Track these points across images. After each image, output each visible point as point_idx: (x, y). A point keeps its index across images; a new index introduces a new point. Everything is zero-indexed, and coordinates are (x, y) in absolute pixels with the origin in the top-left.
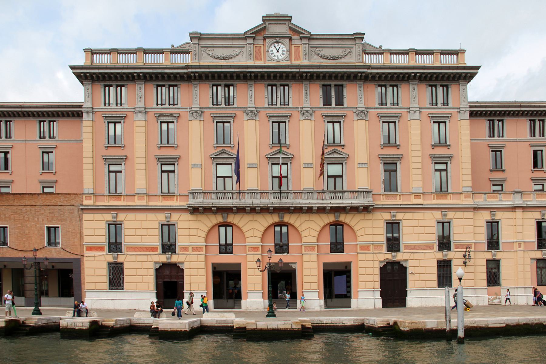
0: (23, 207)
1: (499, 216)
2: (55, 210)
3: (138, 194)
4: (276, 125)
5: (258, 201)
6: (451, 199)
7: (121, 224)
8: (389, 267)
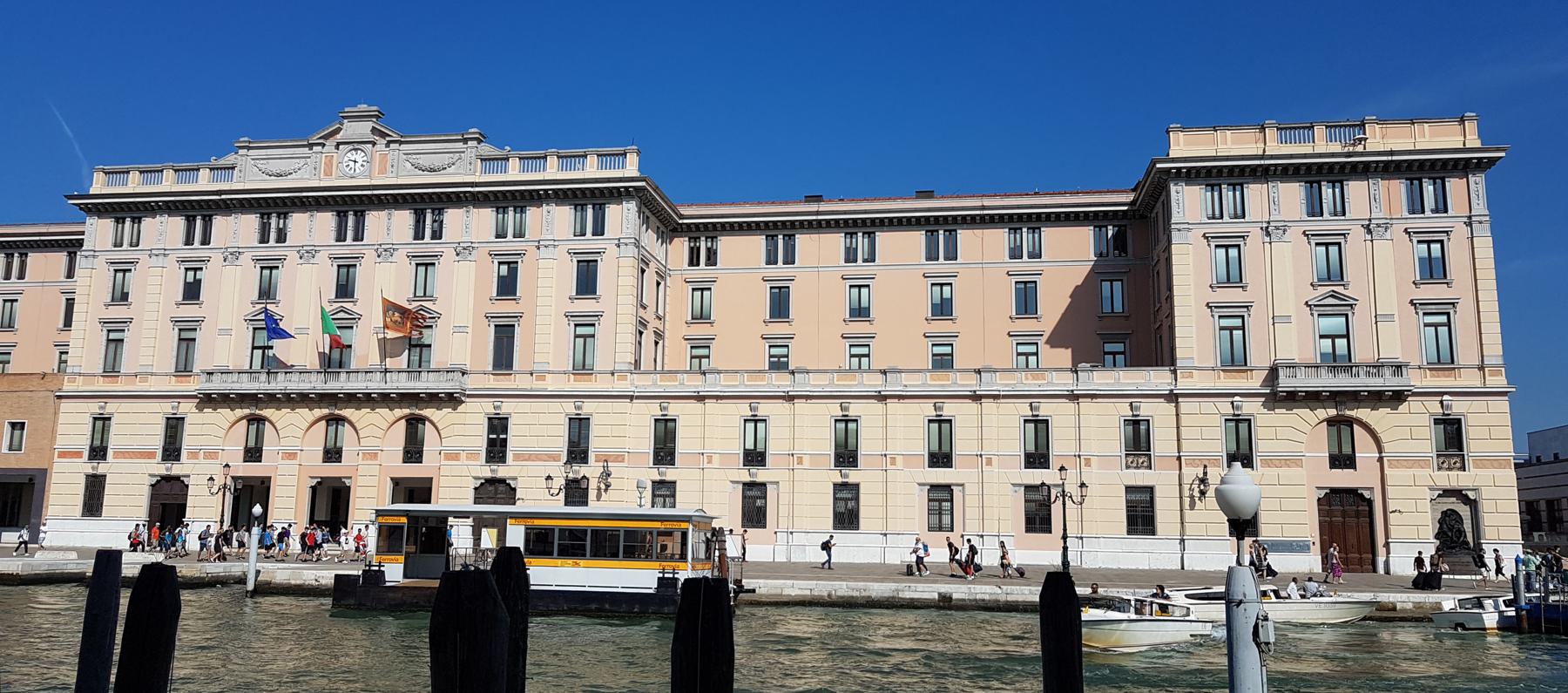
3: (141, 373)
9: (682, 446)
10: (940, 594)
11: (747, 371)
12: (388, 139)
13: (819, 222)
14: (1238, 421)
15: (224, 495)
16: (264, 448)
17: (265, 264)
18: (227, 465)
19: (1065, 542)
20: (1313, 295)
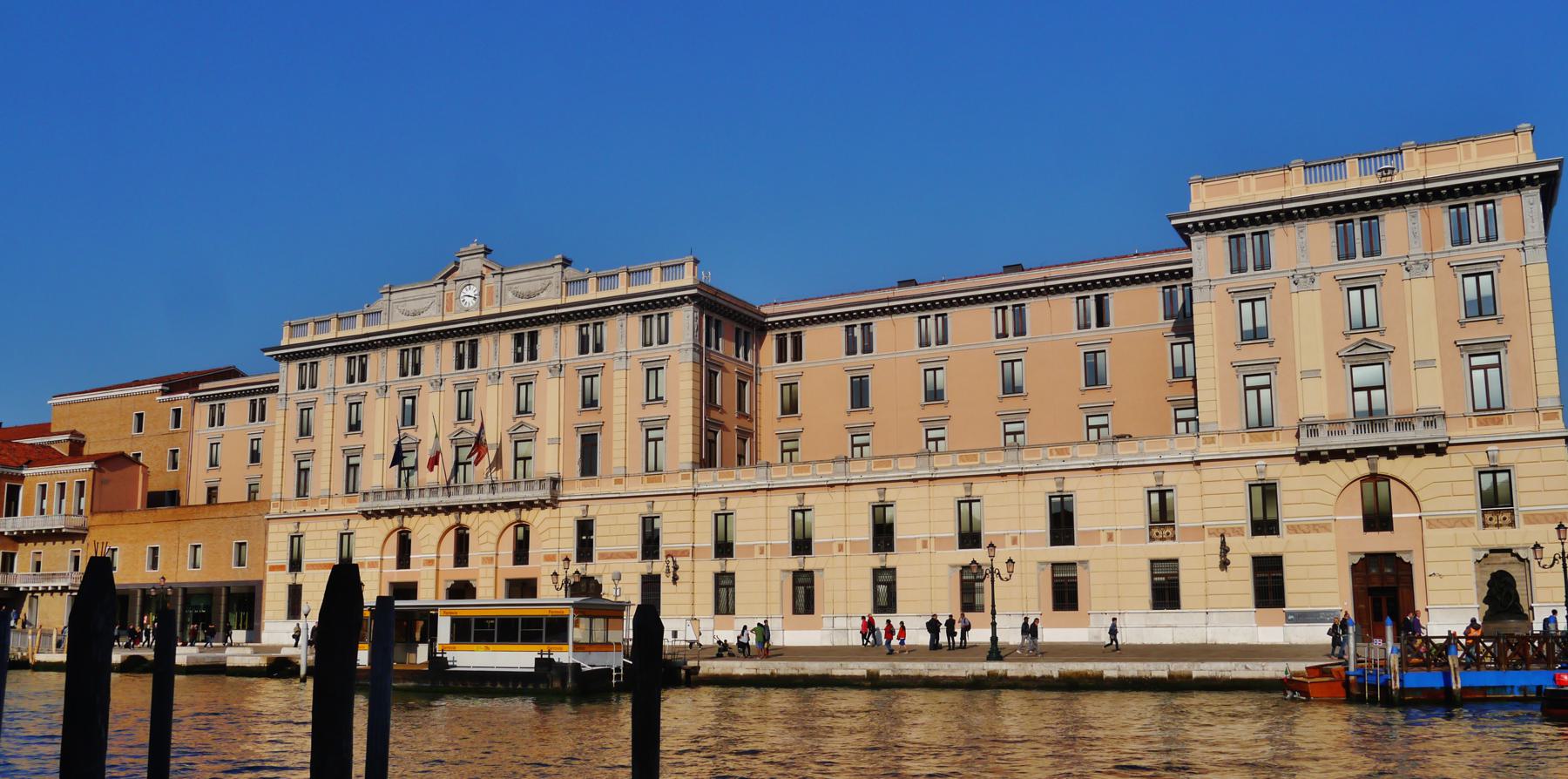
1: (811, 499)
6: (1278, 440)
7: (732, 514)
9: (1081, 524)
10: (868, 671)
11: (985, 450)
13: (1047, 288)
16: (1394, 516)
19: (994, 618)
20: (1344, 345)
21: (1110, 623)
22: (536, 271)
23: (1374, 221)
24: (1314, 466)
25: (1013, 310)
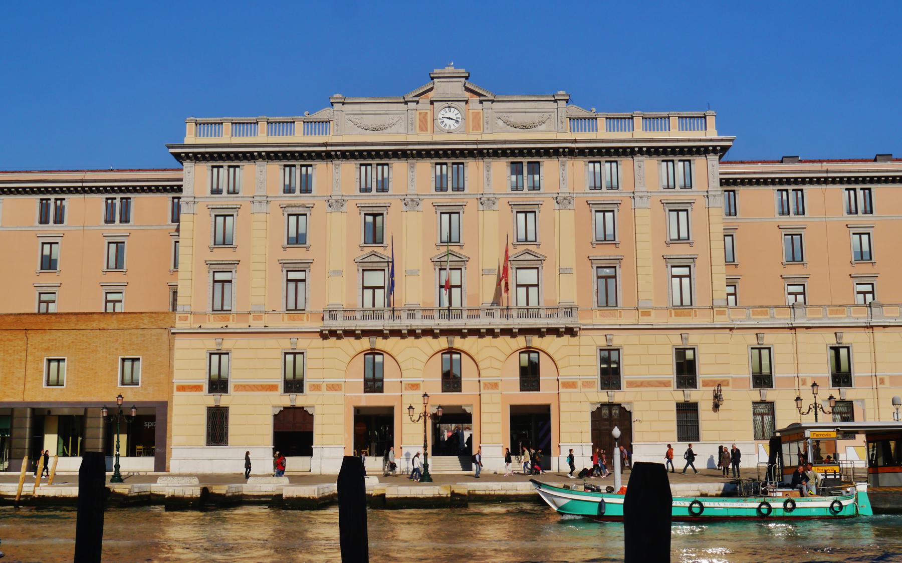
0: (89, 331)
2: (134, 335)
4: (293, 219)
5: (419, 323)
8: (605, 411)
9: (626, 375)
12: (482, 98)
13: (83, 188)
14: (760, 349)
15: (425, 422)
17: (370, 211)
18: (425, 395)
21: (568, 454)
22: (533, 103)
23: (461, 166)
24: (333, 340)
25: (121, 202)
